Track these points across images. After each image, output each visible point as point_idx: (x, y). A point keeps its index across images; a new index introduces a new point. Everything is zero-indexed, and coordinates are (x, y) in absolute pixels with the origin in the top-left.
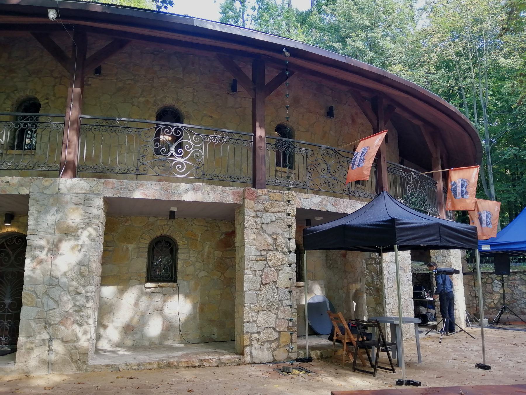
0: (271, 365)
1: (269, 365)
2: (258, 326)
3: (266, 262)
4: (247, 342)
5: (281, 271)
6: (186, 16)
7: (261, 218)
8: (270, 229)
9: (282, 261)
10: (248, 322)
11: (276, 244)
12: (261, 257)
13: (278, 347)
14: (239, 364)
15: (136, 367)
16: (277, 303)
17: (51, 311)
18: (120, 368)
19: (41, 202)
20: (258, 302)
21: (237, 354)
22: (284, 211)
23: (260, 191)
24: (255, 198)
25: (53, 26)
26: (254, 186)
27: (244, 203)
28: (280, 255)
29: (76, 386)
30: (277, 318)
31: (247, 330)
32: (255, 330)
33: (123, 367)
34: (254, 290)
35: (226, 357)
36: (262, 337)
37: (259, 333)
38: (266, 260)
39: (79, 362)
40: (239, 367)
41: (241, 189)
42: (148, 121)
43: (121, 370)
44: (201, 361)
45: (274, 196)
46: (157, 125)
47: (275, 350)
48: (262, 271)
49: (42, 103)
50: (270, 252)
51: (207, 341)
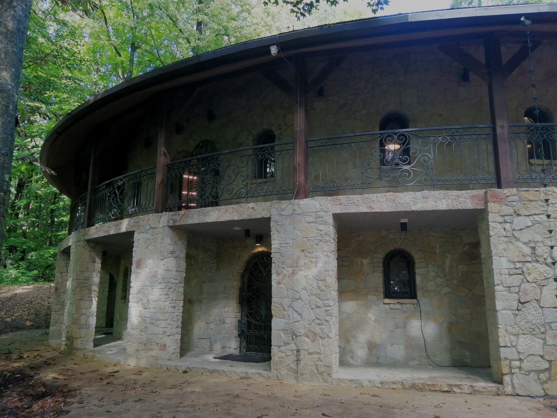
0: (541, 400)
1: (538, 399)
2: (519, 353)
3: (522, 277)
4: (505, 370)
5: (545, 287)
6: (399, 14)
7: (511, 223)
8: (526, 236)
9: (545, 275)
10: (505, 347)
11: (535, 254)
12: (515, 271)
13: (549, 379)
14: (498, 395)
15: (380, 385)
16: (544, 326)
17: (297, 323)
18: (364, 384)
19: (280, 223)
20: (516, 324)
21: (495, 382)
22: (542, 212)
23: (506, 191)
24: (500, 200)
25: (277, 61)
26: (499, 186)
27: (487, 207)
28: (542, 268)
29: (322, 397)
30: (545, 344)
31: (505, 356)
32: (516, 356)
33: (366, 383)
34: (509, 309)
35: (481, 384)
36: (526, 365)
37: (520, 360)
38: (522, 273)
39: (324, 374)
40: (498, 397)
41: (481, 192)
42: (344, 136)
43: (365, 386)
44: (450, 385)
45: (527, 196)
46: (381, 134)
47: (545, 382)
48: (519, 286)
49: (276, 134)
50: (528, 265)
51: (459, 364)
